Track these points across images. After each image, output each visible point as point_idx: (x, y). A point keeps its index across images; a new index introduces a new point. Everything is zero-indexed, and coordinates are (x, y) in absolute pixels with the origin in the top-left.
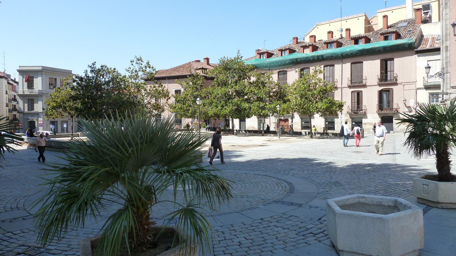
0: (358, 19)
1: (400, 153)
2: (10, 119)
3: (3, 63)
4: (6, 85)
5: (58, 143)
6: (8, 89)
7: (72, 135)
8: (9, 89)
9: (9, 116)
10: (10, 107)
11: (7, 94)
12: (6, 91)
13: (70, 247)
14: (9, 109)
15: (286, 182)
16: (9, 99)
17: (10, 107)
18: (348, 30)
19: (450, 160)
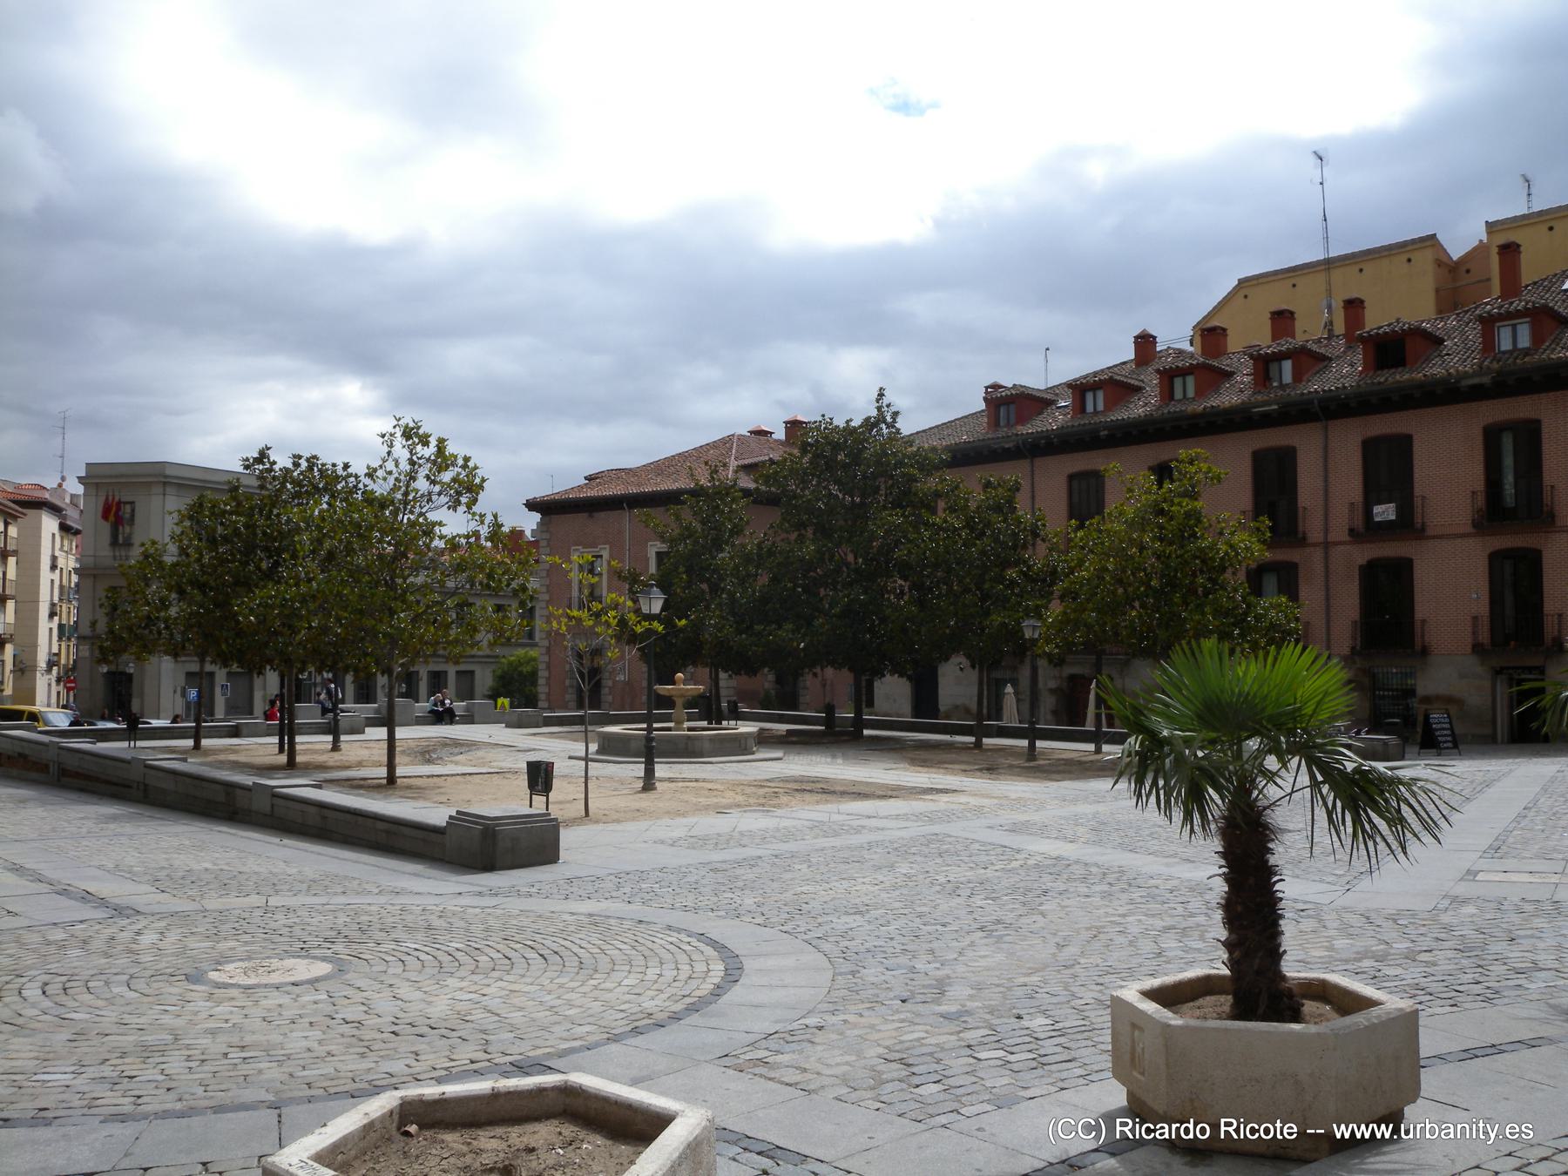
0: (1409, 260)
1: (570, 758)
2: (63, 661)
3: (59, 453)
4: (54, 535)
5: (32, 745)
6: (61, 549)
7: (198, 728)
8: (65, 549)
9: (60, 650)
10: (64, 616)
11: (54, 567)
12: (54, 558)
13: (1086, 1073)
14: (61, 626)
15: (713, 943)
16: (61, 587)
17: (64, 616)
18: (1354, 307)
19: (1271, 845)
